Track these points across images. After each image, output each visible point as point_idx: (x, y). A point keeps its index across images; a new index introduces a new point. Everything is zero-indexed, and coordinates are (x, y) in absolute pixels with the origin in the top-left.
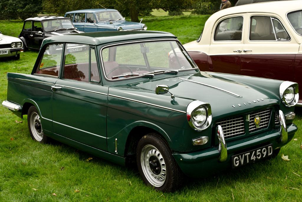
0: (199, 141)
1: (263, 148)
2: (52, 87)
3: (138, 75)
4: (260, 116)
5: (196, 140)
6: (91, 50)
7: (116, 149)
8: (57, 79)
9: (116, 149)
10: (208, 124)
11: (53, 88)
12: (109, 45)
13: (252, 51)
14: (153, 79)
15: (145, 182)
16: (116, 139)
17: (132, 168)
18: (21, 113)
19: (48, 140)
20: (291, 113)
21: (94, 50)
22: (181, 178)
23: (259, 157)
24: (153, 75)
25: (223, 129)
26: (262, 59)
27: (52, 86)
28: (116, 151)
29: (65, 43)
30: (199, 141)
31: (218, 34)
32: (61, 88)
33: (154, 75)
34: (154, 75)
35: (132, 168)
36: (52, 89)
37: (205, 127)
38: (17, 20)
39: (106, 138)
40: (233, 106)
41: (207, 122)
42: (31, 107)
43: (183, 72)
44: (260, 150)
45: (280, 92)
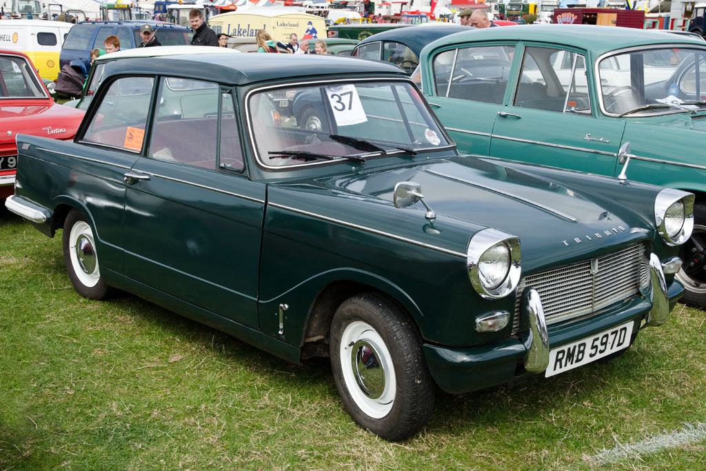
0: (490, 323)
2: (126, 174)
4: (537, 289)
5: (484, 320)
10: (509, 286)
11: (128, 177)
13: (519, 118)
14: (414, 161)
17: (317, 370)
20: (499, 314)
22: (435, 404)
25: (541, 297)
27: (126, 172)
29: (159, 76)
30: (490, 323)
32: (147, 177)
37: (506, 292)
38: (142, 21)
41: (507, 281)
43: (428, 154)
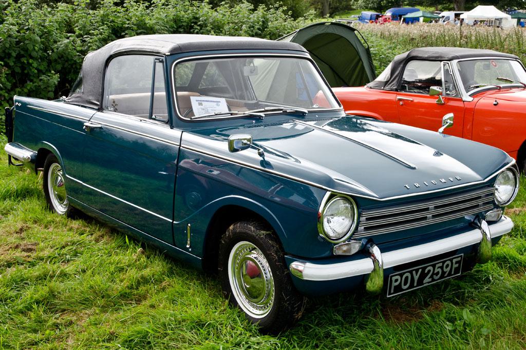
1: (445, 261)
3: (236, 114)
6: (156, 63)
7: (189, 242)
8: (94, 112)
9: (189, 242)
11: (87, 126)
12: (195, 147)
15: (233, 303)
16: (189, 225)
17: (209, 270)
18: (34, 166)
19: (73, 213)
21: (161, 64)
23: (437, 276)
24: (262, 114)
26: (328, 101)
28: (188, 246)
31: (32, 153)
32: (100, 126)
33: (264, 116)
34: (264, 116)
35: (209, 270)
36: (84, 127)
39: (171, 221)
40: (407, 186)
42: (49, 156)
44: (441, 265)
45: (284, 124)
